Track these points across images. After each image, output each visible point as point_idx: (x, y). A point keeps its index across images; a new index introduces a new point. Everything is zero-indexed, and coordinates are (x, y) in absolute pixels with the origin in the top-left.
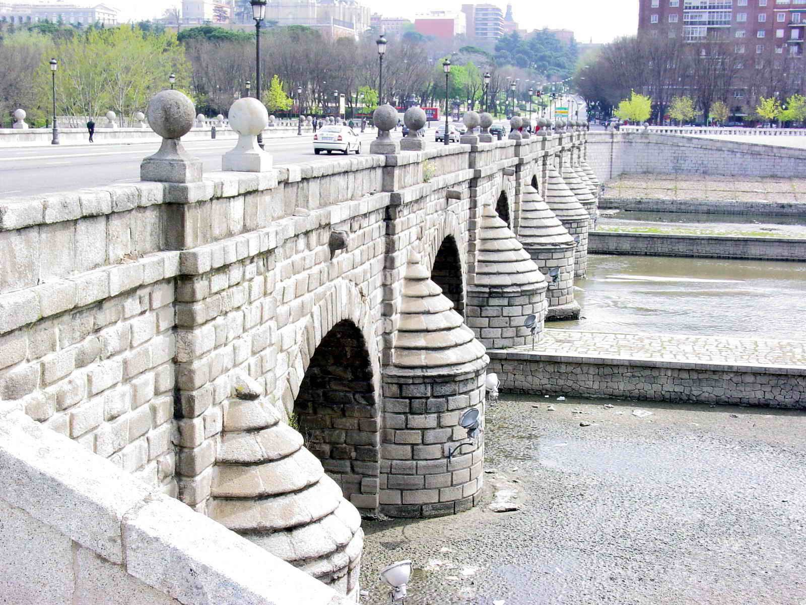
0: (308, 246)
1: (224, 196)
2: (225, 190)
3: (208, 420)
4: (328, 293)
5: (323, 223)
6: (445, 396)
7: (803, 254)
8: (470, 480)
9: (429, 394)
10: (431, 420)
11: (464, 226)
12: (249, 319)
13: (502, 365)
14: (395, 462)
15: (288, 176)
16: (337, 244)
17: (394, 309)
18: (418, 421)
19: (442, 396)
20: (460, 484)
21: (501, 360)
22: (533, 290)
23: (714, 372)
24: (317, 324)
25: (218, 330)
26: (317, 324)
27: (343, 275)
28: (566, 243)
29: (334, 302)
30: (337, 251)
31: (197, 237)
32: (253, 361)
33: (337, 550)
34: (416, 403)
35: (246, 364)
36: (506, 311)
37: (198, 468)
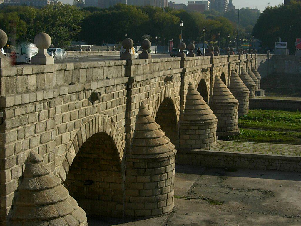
0: (79, 98)
1: (23, 74)
2: (24, 71)
3: (13, 171)
4: (91, 120)
5: (87, 88)
6: (154, 168)
7: (123, 85)
8: (166, 206)
9: (146, 167)
10: (148, 179)
11: (177, 93)
12: (38, 128)
13: (195, 156)
14: (131, 197)
15: (66, 67)
16: (94, 97)
17: (131, 128)
18: (141, 179)
19: (153, 168)
20: (162, 207)
21: (195, 154)
22: (210, 123)
23: (290, 161)
24: (83, 133)
25: (19, 132)
26: (83, 133)
27: (100, 112)
28: (234, 103)
29: (94, 123)
30: (95, 101)
31: (8, 91)
32: (41, 146)
33: (50, 220)
34: (141, 171)
35: (37, 147)
36: (197, 132)
37: (7, 192)
